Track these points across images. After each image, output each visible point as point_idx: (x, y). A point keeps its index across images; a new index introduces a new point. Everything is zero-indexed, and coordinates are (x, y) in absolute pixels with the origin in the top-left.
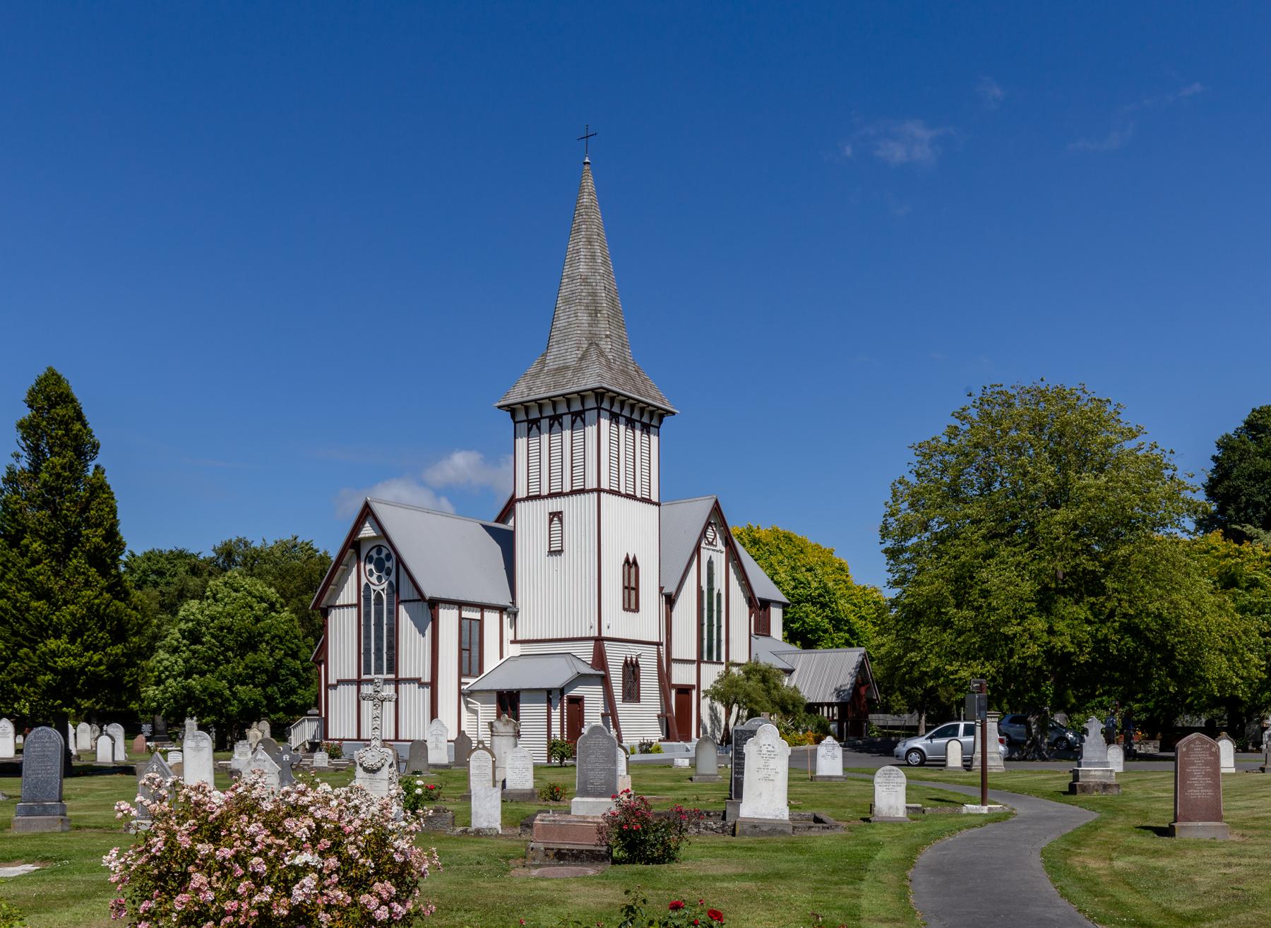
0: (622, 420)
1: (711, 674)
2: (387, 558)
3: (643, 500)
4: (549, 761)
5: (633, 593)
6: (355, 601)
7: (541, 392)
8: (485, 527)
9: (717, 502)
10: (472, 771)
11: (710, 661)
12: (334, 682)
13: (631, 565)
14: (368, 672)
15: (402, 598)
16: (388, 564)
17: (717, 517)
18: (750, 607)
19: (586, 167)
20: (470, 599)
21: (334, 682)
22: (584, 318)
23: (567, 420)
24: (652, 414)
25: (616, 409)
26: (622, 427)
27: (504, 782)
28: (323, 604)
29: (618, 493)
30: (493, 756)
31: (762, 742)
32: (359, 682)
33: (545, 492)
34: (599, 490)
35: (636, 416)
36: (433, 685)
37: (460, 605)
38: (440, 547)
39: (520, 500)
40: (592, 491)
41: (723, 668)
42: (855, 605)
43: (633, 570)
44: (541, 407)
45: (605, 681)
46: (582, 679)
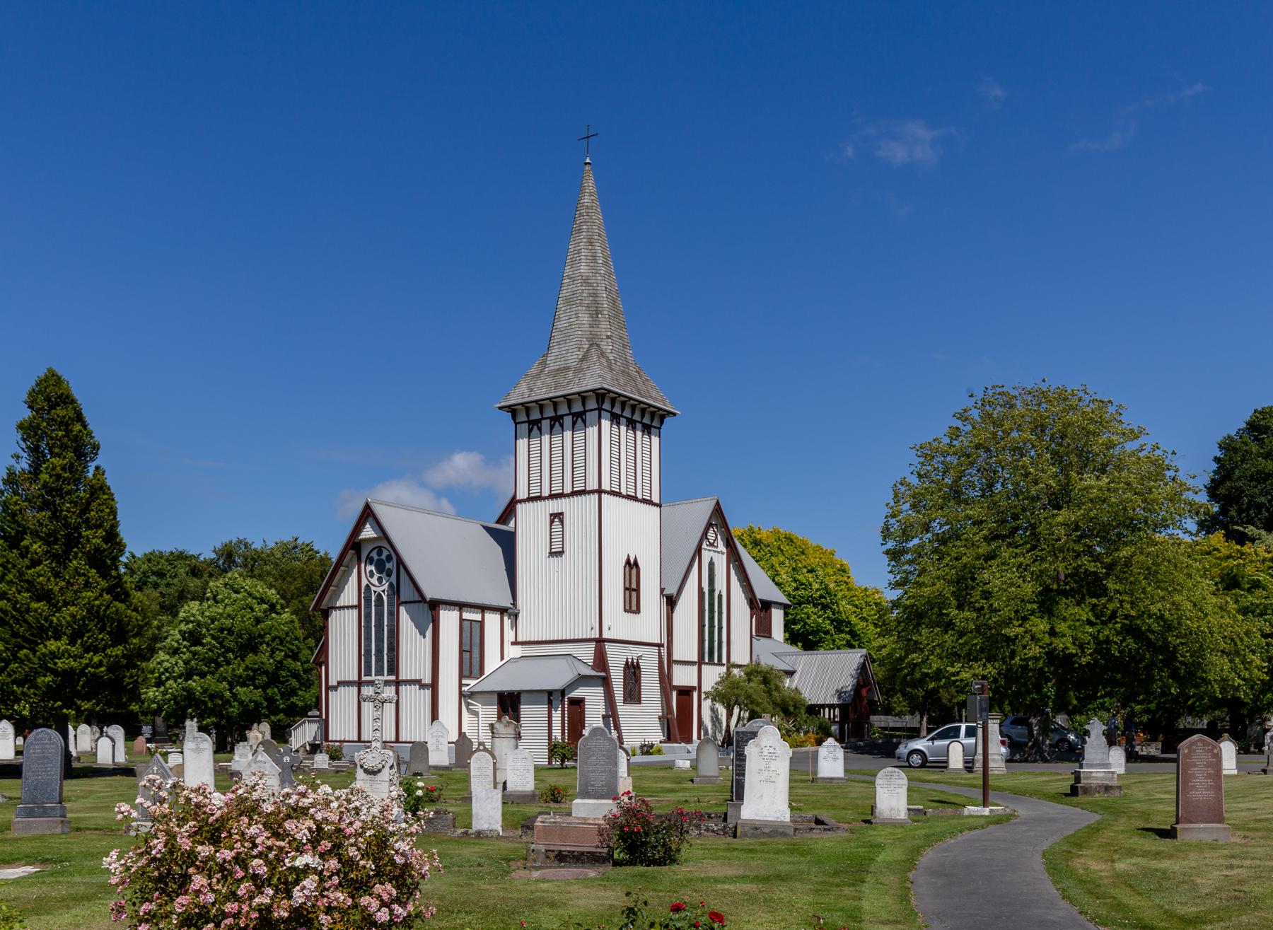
0: (623, 420)
1: (712, 676)
2: (388, 559)
3: (644, 501)
4: (550, 763)
5: (634, 594)
6: (355, 603)
7: (542, 393)
8: (486, 528)
9: (718, 503)
10: (473, 773)
11: (711, 662)
12: (335, 684)
13: (632, 566)
14: (368, 673)
15: (402, 599)
16: (388, 566)
17: (718, 518)
18: (751, 608)
19: (587, 168)
20: (471, 600)
21: (335, 684)
22: (585, 318)
23: (568, 421)
24: (653, 415)
25: (617, 410)
26: (623, 428)
27: (505, 783)
28: (324, 606)
29: (619, 494)
30: (494, 757)
31: (763, 744)
32: (359, 684)
33: (546, 493)
34: (600, 491)
35: (637, 417)
36: (434, 686)
37: (461, 606)
38: (440, 549)
39: (521, 501)
40: (593, 492)
41: (724, 669)
42: (856, 606)
43: (634, 571)
44: (541, 408)
45: (606, 682)
46: (583, 680)
